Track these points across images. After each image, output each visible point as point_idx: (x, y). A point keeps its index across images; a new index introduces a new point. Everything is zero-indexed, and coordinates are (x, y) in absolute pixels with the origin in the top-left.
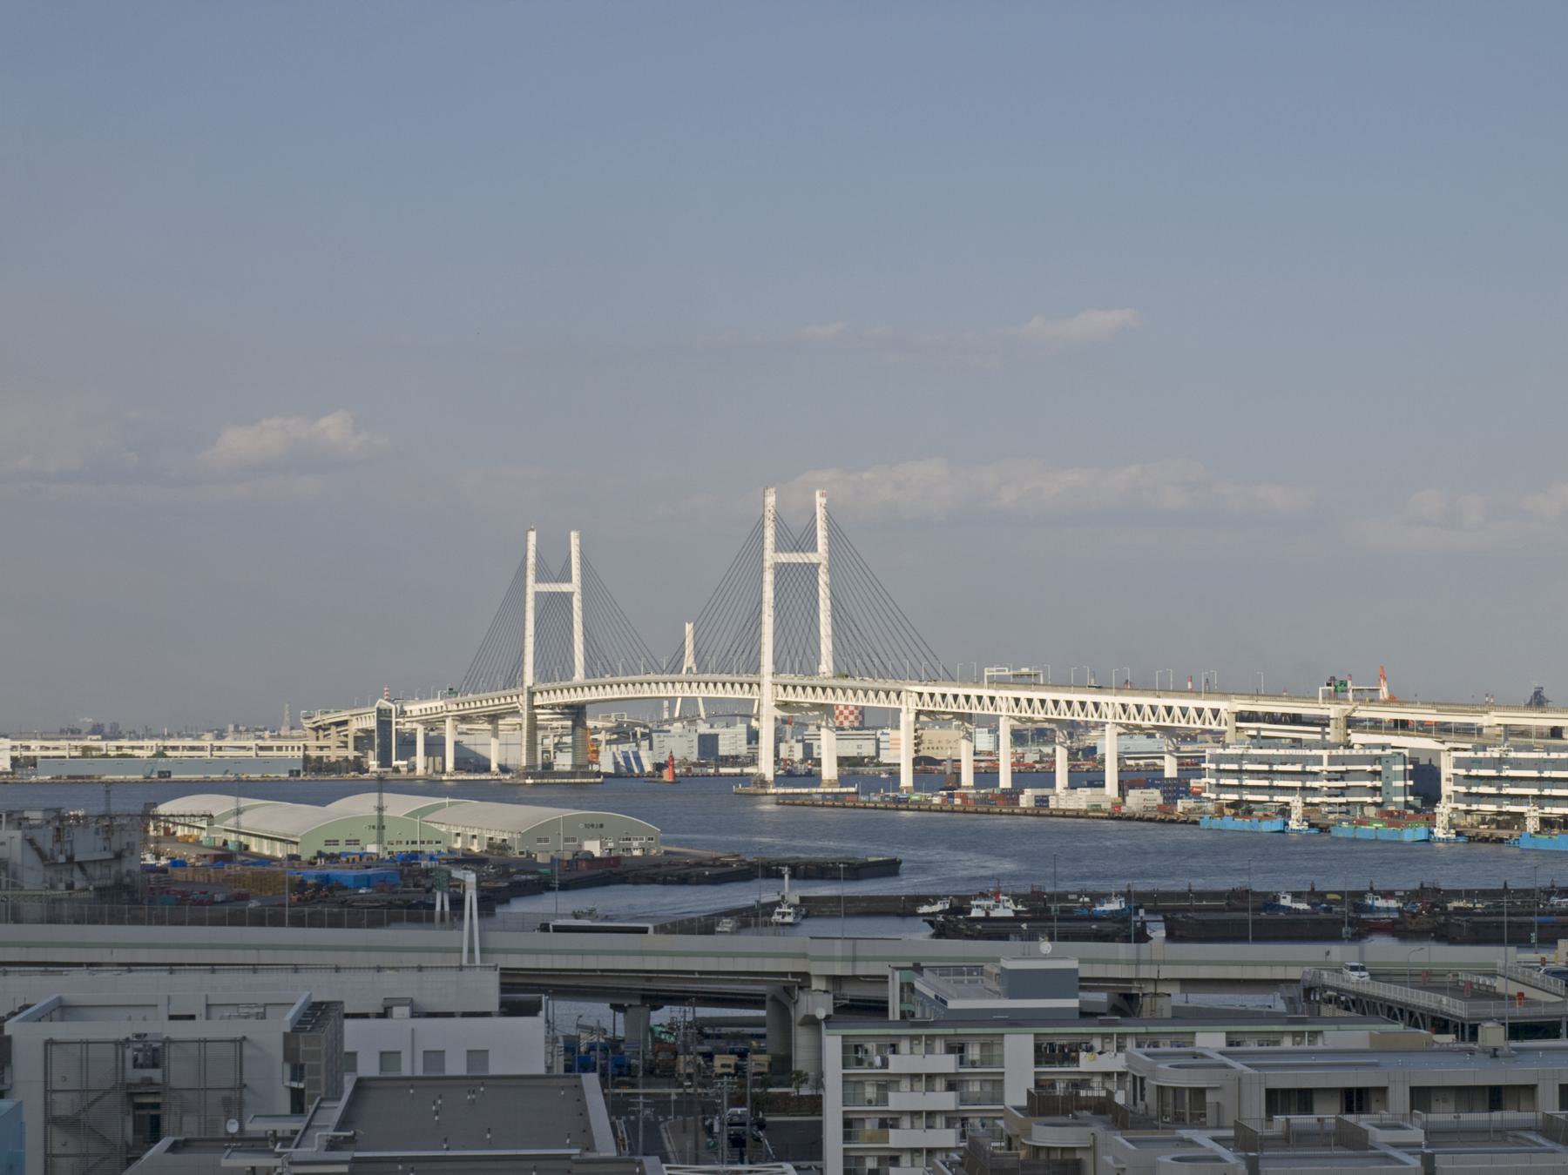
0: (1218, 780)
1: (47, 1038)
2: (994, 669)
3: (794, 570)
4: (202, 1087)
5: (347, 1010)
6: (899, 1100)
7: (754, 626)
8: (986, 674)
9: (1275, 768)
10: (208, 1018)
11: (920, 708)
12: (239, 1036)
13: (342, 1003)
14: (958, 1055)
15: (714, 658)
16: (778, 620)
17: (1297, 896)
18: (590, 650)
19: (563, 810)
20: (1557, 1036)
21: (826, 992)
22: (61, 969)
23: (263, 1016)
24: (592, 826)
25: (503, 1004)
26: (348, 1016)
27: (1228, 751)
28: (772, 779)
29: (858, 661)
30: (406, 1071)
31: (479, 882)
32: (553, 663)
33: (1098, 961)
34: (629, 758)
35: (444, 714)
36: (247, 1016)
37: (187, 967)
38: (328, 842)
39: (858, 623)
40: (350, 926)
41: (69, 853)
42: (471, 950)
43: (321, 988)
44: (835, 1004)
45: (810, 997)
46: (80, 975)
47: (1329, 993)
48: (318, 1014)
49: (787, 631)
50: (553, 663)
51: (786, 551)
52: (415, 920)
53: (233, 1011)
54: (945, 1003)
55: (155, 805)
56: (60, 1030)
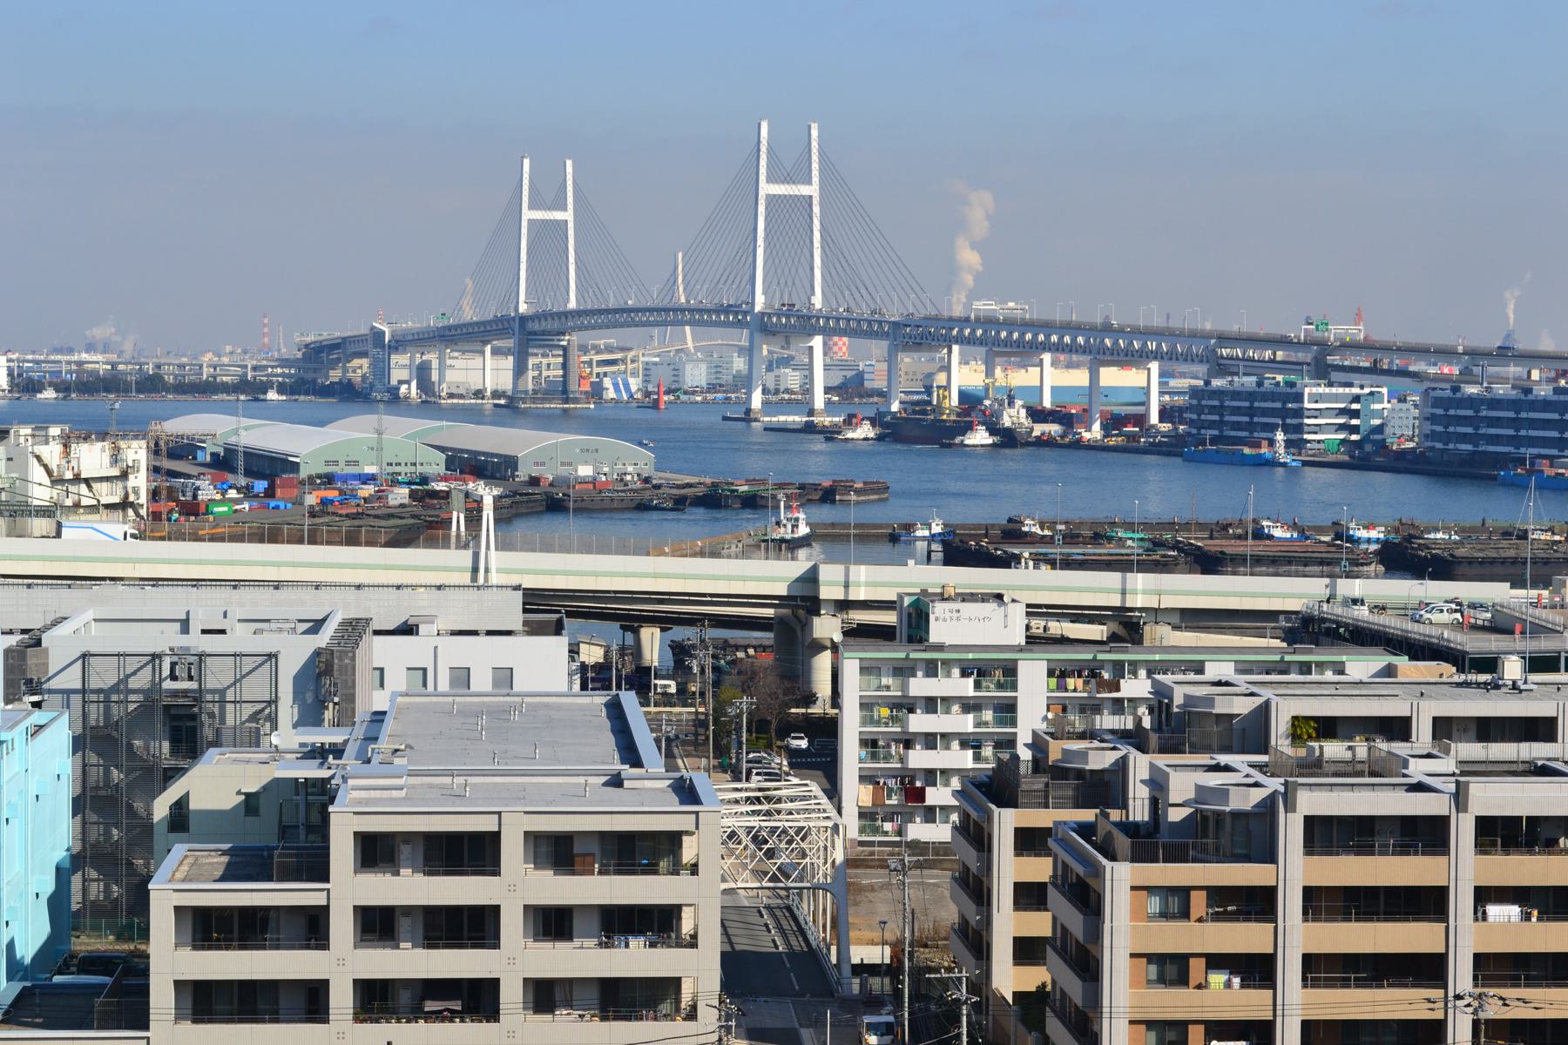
2: (981, 303)
4: (238, 705)
6: (919, 722)
16: (769, 251)
18: (582, 278)
20: (1557, 670)
24: (588, 450)
25: (525, 623)
28: (760, 406)
29: (847, 293)
32: (544, 290)
34: (618, 384)
37: (209, 583)
38: (327, 463)
39: (847, 255)
41: (76, 470)
47: (1327, 625)
49: (777, 261)
50: (544, 290)
51: (777, 183)
52: (432, 543)
55: (993, 445)
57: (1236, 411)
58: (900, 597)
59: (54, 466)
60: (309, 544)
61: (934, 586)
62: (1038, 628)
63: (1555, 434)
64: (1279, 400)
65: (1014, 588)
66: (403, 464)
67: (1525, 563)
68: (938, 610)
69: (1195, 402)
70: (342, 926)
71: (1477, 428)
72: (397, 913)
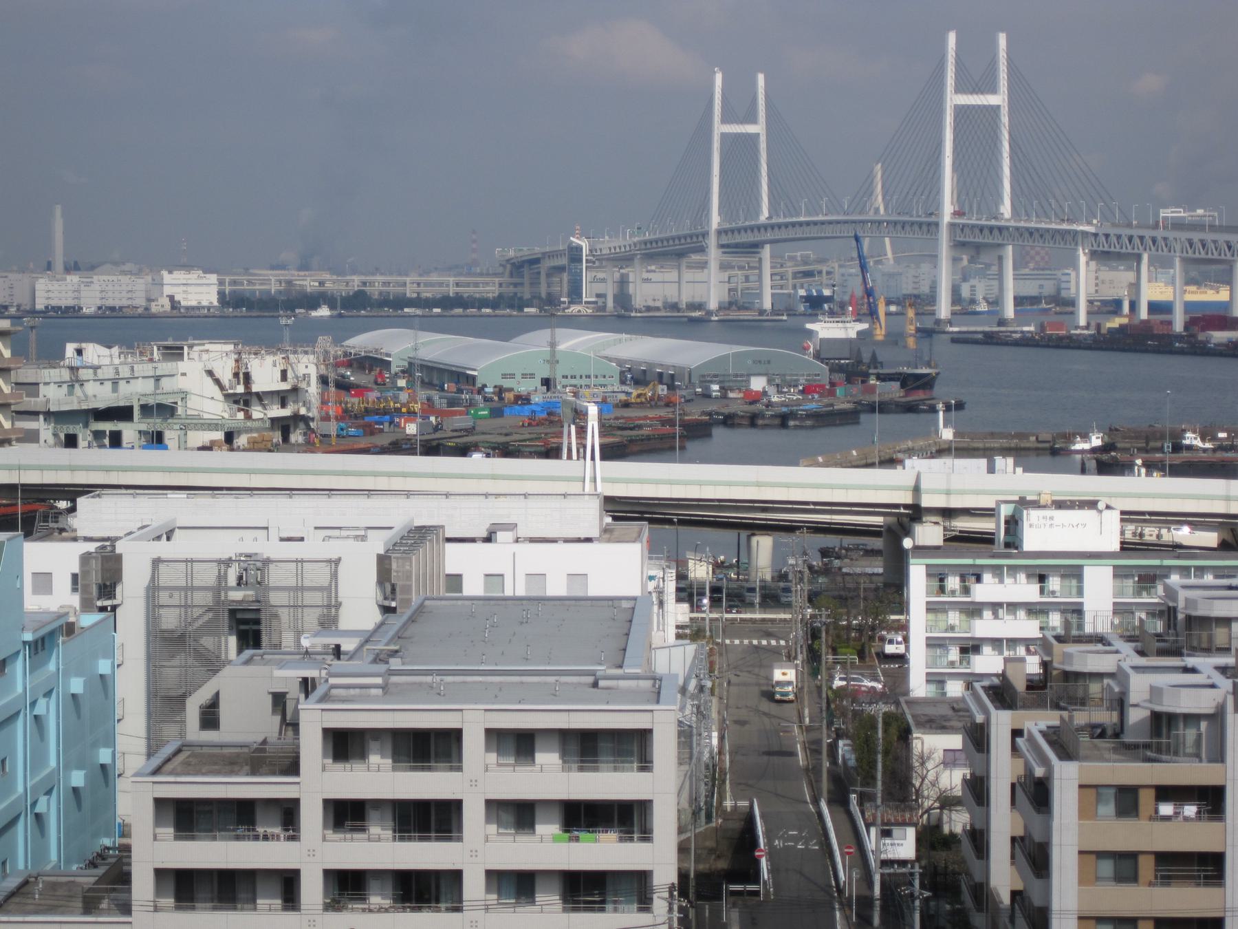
1: (155, 556)
2: (1169, 210)
3: (974, 112)
4: (300, 610)
5: (448, 535)
8: (1162, 215)
11: (1095, 248)
12: (334, 556)
13: (443, 527)
14: (1038, 585)
15: (895, 197)
19: (734, 346)
22: (165, 492)
23: (363, 538)
24: (760, 362)
26: (449, 540)
30: (508, 592)
31: (600, 412)
35: (632, 253)
36: (348, 537)
38: (504, 376)
43: (423, 513)
46: (433, 503)
48: (420, 535)
56: (163, 549)
58: (999, 503)
59: (226, 383)
61: (1031, 493)
62: (1151, 535)
65: (1110, 495)
66: (578, 377)
67: (674, 438)
68: (1031, 518)
70: (312, 817)
72: (367, 807)
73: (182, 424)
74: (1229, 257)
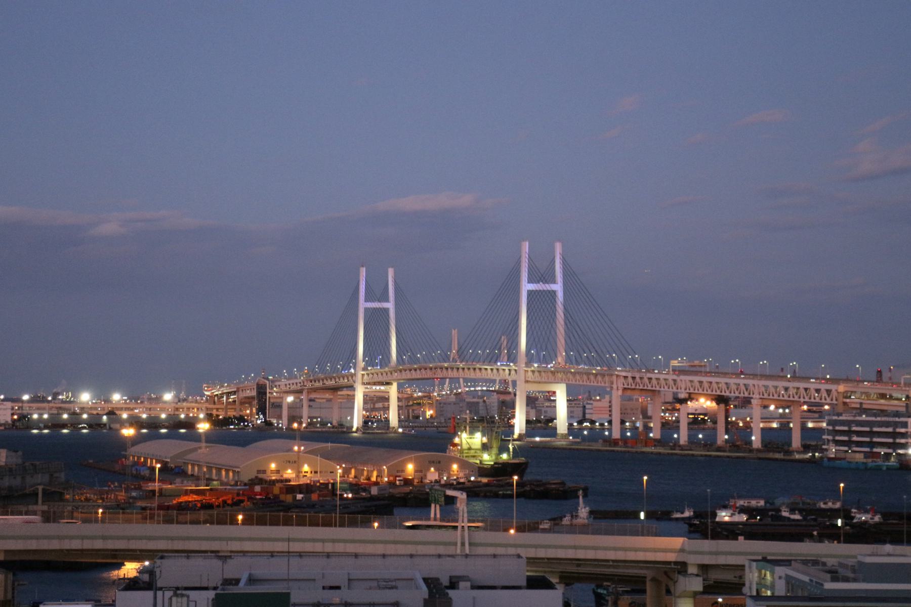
0: (834, 437)
7: (514, 329)
8: (672, 364)
9: (875, 429)
10: (349, 588)
11: (626, 386)
17: (792, 511)
21: (697, 575)
24: (433, 462)
27: (841, 418)
33: (549, 547)
37: (256, 554)
40: (271, 524)
42: (463, 544)
44: (704, 584)
45: (687, 579)
53: (375, 584)
54: (822, 585)
57: (859, 434)
60: (309, 526)
63: (891, 440)
64: (891, 426)
69: (830, 428)
71: (850, 437)
73: (74, 506)
74: (658, 388)
